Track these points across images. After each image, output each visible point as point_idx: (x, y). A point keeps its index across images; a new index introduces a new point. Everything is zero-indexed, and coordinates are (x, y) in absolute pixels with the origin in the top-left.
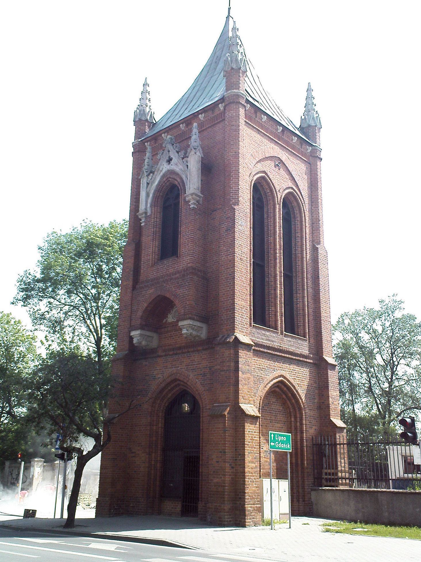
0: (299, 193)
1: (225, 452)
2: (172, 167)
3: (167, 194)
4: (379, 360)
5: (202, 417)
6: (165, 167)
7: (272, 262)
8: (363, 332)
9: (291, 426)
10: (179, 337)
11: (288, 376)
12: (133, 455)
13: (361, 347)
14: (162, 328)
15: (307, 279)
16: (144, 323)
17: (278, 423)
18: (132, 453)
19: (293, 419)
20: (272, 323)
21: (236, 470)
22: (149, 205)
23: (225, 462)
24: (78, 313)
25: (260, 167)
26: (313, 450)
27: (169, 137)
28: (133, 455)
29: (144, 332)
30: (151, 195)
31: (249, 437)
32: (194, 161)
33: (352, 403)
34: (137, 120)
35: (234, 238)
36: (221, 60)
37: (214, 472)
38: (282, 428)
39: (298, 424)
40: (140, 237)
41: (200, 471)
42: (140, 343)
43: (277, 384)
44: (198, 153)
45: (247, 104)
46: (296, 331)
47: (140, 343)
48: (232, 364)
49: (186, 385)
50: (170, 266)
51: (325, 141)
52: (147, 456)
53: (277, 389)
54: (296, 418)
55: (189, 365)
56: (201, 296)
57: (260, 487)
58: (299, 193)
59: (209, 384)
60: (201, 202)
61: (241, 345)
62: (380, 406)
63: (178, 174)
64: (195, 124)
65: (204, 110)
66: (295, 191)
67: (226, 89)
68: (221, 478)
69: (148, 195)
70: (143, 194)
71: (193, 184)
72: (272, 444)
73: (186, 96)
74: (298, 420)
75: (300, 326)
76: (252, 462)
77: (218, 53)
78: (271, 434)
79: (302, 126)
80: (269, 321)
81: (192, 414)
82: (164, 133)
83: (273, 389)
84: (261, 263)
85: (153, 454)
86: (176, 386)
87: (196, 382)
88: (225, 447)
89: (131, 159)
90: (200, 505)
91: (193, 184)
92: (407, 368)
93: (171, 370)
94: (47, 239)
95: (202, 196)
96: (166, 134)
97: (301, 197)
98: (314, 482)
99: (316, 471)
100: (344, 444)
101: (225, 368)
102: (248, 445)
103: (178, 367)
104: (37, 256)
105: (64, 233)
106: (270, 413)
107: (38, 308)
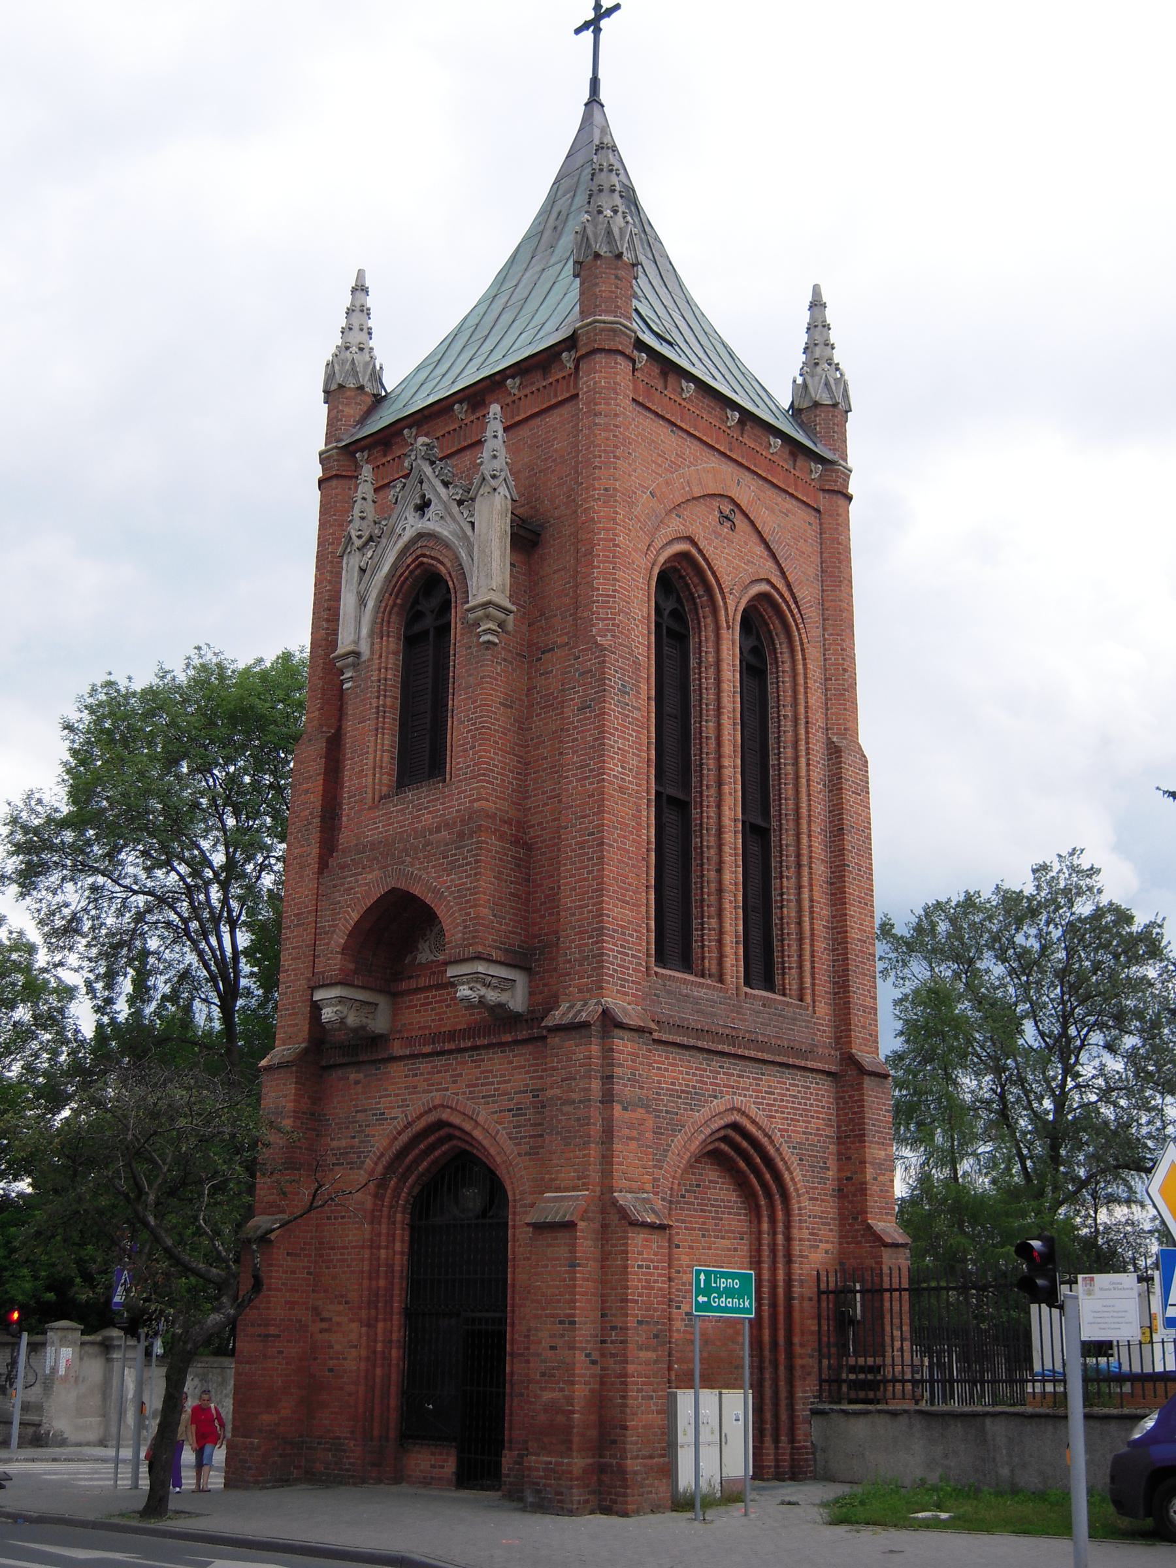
0: (787, 595)
1: (574, 1323)
2: (431, 523)
3: (416, 602)
4: (1030, 1035)
5: (514, 1227)
6: (411, 525)
7: (713, 791)
8: (988, 954)
9: (760, 1244)
10: (448, 1006)
11: (753, 1110)
12: (325, 1325)
13: (979, 1002)
15: (810, 836)
16: (352, 966)
17: (723, 1238)
18: (322, 1320)
19: (765, 1226)
20: (710, 964)
21: (602, 1369)
22: (365, 631)
23: (572, 1348)
24: (173, 916)
25: (675, 526)
26: (819, 1307)
27: (422, 440)
30: (371, 604)
31: (640, 1280)
32: (493, 519)
33: (951, 1159)
34: (334, 387)
35: (601, 729)
36: (570, 223)
37: (543, 1374)
38: (736, 1250)
39: (780, 1238)
40: (340, 720)
41: (508, 1369)
42: (342, 1021)
43: (722, 1133)
44: (503, 490)
45: (640, 351)
46: (778, 979)
47: (342, 1021)
48: (596, 1085)
49: (466, 1138)
50: (429, 807)
51: (864, 451)
52: (364, 1329)
53: (723, 1146)
54: (773, 1221)
56: (511, 894)
57: (670, 1412)
58: (787, 595)
59: (531, 1137)
60: (510, 626)
61: (617, 1032)
62: (1029, 1163)
63: (447, 545)
64: (495, 408)
65: (522, 369)
66: (777, 590)
67: (582, 312)
68: (562, 1390)
69: (362, 601)
70: (348, 601)
71: (489, 576)
72: (701, 1299)
73: (472, 322)
74: (780, 1227)
75: (790, 968)
77: (562, 204)
78: (698, 1272)
79: (796, 404)
80: (703, 958)
82: (410, 427)
83: (711, 1147)
84: (680, 796)
85: (380, 1325)
86: (441, 1141)
87: (494, 1131)
88: (575, 1308)
89: (314, 497)
90: (507, 1460)
91: (489, 576)
92: (1107, 1058)
93: (425, 1097)
94: (90, 701)
95: (514, 608)
96: (414, 430)
97: (793, 606)
98: (821, 1391)
99: (825, 1362)
100: (900, 1290)
101: (574, 1096)
102: (636, 1302)
103: (447, 1089)
104: (60, 750)
105: (138, 686)
107: (59, 898)
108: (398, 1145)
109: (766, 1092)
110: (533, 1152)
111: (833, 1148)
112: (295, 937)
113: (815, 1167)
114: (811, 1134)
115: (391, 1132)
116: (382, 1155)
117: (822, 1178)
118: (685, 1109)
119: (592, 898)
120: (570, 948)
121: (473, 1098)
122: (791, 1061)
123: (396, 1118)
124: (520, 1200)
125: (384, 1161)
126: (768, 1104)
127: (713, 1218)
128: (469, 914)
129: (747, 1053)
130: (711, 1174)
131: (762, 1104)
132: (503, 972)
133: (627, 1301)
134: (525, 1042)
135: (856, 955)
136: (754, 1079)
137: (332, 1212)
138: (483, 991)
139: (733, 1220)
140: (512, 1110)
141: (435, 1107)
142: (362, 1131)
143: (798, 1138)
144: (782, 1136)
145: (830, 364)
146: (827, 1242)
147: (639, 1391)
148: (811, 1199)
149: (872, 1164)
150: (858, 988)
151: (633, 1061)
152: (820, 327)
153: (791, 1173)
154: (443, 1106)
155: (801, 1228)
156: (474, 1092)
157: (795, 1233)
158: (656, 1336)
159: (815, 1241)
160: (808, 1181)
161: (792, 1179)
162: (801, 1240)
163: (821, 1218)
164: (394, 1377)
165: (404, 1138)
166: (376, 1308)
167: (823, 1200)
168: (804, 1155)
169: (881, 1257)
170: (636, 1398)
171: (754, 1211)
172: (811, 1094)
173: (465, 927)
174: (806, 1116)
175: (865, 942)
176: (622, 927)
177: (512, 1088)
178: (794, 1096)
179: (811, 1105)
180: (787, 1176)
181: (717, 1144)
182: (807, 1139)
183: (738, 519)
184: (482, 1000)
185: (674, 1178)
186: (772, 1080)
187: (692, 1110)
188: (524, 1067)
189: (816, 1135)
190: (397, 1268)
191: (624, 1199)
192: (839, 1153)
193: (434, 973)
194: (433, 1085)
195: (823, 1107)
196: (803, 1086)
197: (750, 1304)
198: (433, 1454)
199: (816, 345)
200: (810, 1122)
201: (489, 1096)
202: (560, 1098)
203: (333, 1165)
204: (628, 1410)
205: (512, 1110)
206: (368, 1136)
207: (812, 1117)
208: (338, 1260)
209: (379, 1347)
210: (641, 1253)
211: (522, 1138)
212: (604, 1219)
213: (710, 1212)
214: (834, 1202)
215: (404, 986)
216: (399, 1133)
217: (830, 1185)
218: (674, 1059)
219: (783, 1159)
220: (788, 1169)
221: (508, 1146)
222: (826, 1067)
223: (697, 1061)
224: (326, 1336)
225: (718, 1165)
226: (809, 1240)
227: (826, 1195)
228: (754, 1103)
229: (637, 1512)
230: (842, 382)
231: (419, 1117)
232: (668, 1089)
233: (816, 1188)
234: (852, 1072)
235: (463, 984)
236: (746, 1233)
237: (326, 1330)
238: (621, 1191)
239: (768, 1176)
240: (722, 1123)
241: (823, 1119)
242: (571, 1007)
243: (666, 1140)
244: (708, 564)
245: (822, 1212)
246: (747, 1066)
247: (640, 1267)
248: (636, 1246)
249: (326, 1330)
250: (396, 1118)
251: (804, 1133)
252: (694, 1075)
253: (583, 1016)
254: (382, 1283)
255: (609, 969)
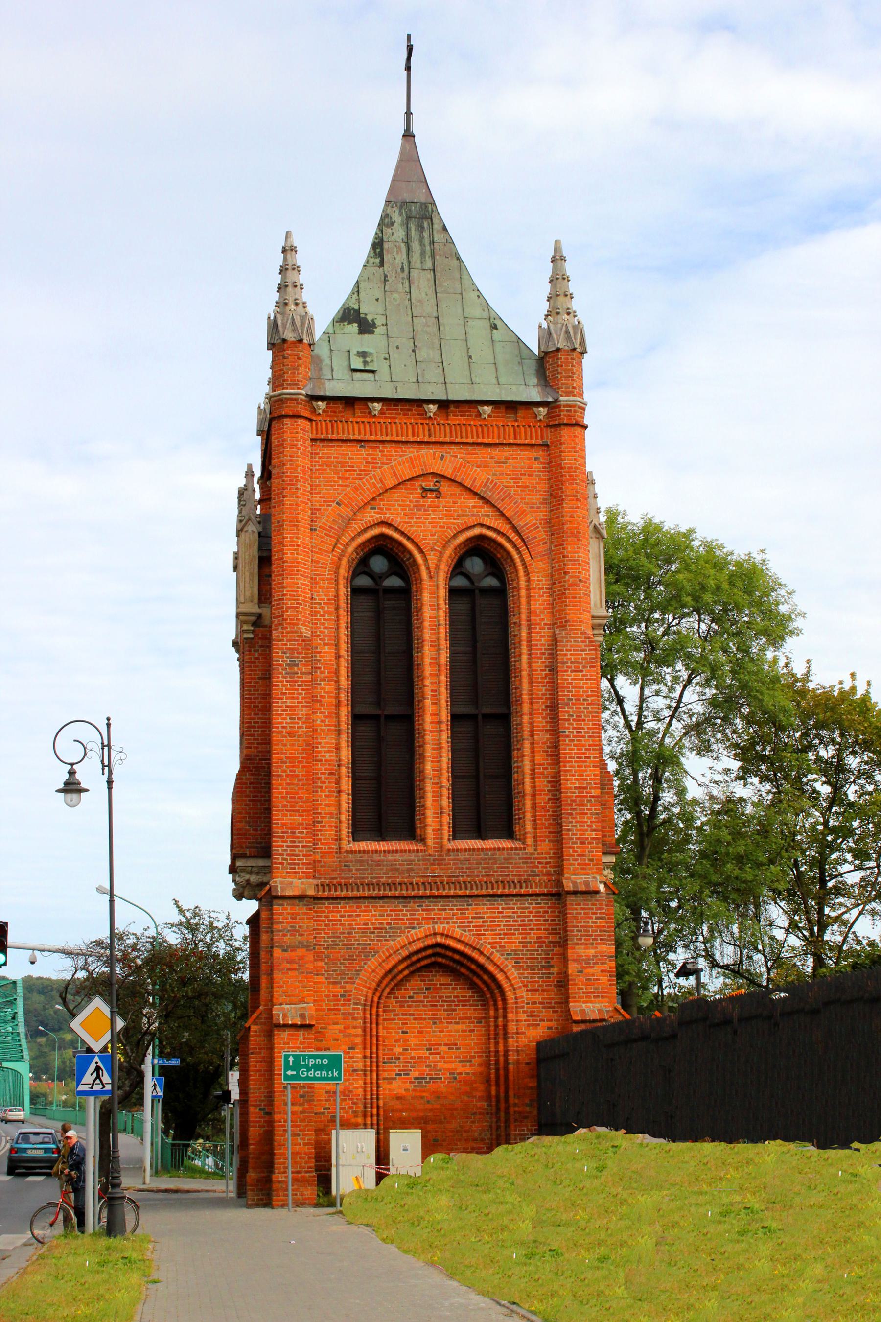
46: (516, 828)
61: (275, 902)
145: (568, 314)
152: (560, 280)
171: (485, 1004)
183: (445, 487)
199: (558, 295)
223: (388, 907)
228: (458, 927)
230: (578, 327)
244: (402, 533)
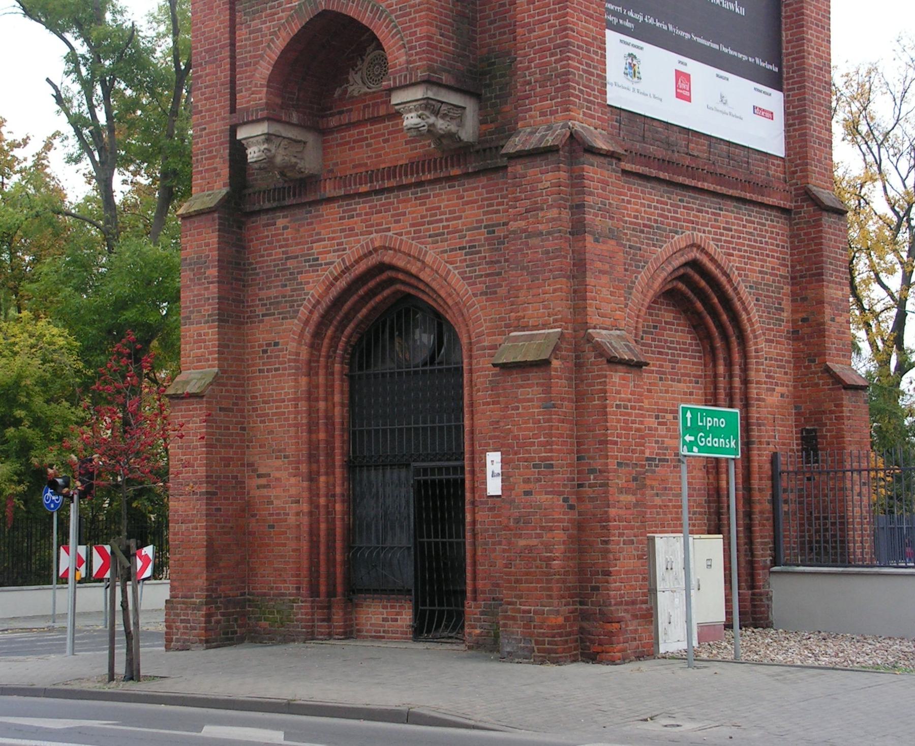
9: (716, 388)
10: (385, 141)
11: (712, 247)
12: (263, 481)
14: (332, 115)
16: (279, 101)
17: (679, 381)
18: (259, 476)
19: (721, 369)
21: (580, 514)
28: (263, 481)
29: (277, 128)
31: (618, 421)
38: (691, 394)
39: (737, 382)
43: (682, 271)
47: (270, 160)
53: (681, 286)
54: (729, 364)
55: (423, 224)
57: (648, 555)
59: (487, 275)
74: (737, 370)
76: (628, 491)
78: (685, 410)
81: (432, 363)
83: (669, 287)
85: (322, 479)
102: (616, 443)
103: (389, 230)
106: (660, 353)
108: (334, 292)
109: (724, 229)
110: (490, 293)
111: (787, 289)
112: (207, 75)
113: (771, 307)
114: (766, 273)
115: (327, 278)
116: (318, 302)
117: (777, 319)
118: (648, 245)
119: (554, 11)
120: (529, 68)
121: (419, 238)
122: (748, 196)
123: (332, 263)
124: (478, 342)
125: (321, 309)
126: (726, 241)
127: (670, 361)
128: (415, 33)
129: (706, 186)
130: (667, 315)
131: (720, 240)
132: (455, 99)
133: (606, 442)
134: (477, 173)
135: (814, 84)
136: (713, 214)
137: (264, 364)
138: (432, 120)
139: (689, 363)
140: (464, 248)
141: (376, 250)
142: (294, 279)
143: (754, 277)
144: (740, 275)
146: (782, 385)
147: (621, 535)
148: (767, 341)
149: (830, 304)
150: (814, 119)
151: (604, 189)
153: (748, 313)
154: (385, 248)
155: (757, 371)
156: (420, 231)
157: (753, 375)
158: (635, 479)
159: (771, 383)
160: (764, 322)
161: (749, 320)
162: (758, 382)
163: (776, 360)
164: (339, 530)
165: (342, 284)
166: (318, 461)
167: (778, 342)
168: (761, 295)
169: (842, 399)
170: (618, 543)
172: (766, 231)
173: (411, 48)
174: (762, 254)
175: (821, 69)
176: (587, 43)
177: (464, 224)
178: (751, 234)
179: (766, 243)
180: (744, 316)
181: (675, 283)
182: (763, 279)
184: (431, 129)
185: (638, 317)
186: (730, 215)
187: (654, 245)
188: (476, 201)
189: (772, 274)
190: (338, 420)
191: (601, 335)
192: (793, 294)
193: (368, 106)
194: (372, 226)
195: (777, 246)
196: (759, 223)
197: (736, 444)
198: (384, 607)
200: (765, 261)
201: (437, 235)
202: (525, 231)
203: (263, 315)
204: (611, 556)
205: (464, 248)
206: (301, 283)
207: (768, 256)
208: (274, 414)
209: (322, 501)
210: (618, 392)
211: (477, 277)
212: (577, 357)
213: (667, 354)
214: (788, 344)
215: (333, 122)
216: (336, 279)
217: (785, 327)
218: (636, 190)
219: (740, 299)
220: (745, 309)
221: (462, 287)
222: (782, 203)
224: (265, 492)
225: (674, 306)
226: (766, 383)
227: (780, 336)
228: (713, 239)
229: (624, 660)
231: (357, 262)
232: (631, 223)
233: (772, 330)
234: (807, 209)
235: (410, 111)
236: (700, 377)
237: (264, 486)
238: (595, 328)
239: (725, 317)
240: (682, 260)
241: (778, 258)
242: (532, 133)
243: (630, 277)
245: (778, 354)
246: (706, 201)
247: (618, 406)
248: (614, 384)
249: (264, 486)
250: (332, 263)
251: (760, 272)
252: (656, 208)
253: (550, 141)
254: (322, 436)
255: (574, 89)
